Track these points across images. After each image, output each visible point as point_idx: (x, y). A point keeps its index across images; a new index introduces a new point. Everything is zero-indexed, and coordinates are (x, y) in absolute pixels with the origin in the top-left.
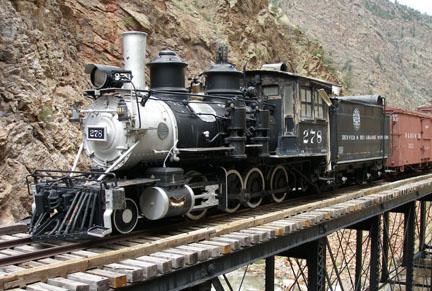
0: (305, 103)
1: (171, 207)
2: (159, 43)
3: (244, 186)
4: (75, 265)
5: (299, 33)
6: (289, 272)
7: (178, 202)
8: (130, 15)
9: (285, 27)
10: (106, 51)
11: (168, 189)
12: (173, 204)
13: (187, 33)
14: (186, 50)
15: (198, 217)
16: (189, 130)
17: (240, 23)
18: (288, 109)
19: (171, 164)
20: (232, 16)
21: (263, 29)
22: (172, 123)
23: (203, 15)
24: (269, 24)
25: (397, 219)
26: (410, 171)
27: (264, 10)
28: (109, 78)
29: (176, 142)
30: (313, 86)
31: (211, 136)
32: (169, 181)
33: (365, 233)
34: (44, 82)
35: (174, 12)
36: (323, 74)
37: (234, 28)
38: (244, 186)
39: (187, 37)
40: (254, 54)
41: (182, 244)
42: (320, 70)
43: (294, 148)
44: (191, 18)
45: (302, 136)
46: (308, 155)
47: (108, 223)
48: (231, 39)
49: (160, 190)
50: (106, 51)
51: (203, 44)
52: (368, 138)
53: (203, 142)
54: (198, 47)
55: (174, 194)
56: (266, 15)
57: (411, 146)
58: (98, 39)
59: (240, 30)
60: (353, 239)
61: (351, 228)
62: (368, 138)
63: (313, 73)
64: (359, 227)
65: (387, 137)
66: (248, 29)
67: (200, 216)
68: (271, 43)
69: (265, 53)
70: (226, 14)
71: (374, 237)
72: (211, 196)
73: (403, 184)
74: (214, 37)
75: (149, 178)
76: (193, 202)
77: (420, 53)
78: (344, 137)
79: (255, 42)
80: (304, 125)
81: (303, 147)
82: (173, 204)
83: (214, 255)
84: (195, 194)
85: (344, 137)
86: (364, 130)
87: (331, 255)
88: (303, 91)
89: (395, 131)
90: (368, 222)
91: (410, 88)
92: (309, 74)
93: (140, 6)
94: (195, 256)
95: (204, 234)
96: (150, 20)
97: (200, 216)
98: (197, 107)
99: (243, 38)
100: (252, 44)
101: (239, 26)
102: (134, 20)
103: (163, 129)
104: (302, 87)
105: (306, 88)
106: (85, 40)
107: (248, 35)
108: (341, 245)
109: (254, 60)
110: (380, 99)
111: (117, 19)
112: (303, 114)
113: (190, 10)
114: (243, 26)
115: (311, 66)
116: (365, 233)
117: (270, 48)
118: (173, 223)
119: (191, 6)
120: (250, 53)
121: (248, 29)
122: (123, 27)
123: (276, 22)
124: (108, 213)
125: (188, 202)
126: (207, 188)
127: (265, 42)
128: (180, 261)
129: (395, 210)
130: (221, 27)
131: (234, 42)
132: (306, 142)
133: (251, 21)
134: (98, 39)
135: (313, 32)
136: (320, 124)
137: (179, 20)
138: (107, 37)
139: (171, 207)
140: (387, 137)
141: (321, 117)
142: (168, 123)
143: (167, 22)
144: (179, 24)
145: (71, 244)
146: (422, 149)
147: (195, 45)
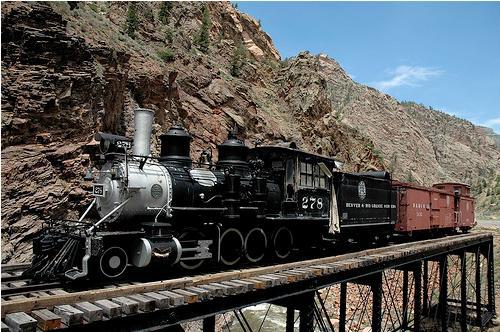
0: (306, 174)
1: (154, 257)
3: (244, 243)
4: (18, 305)
5: (355, 133)
6: (271, 316)
7: (165, 253)
8: (229, 116)
9: (345, 127)
10: (211, 141)
11: (152, 241)
12: (157, 254)
15: (192, 268)
16: (184, 191)
18: (289, 178)
19: (163, 218)
20: (305, 119)
21: (327, 128)
22: (166, 182)
23: (284, 117)
24: (332, 124)
25: (433, 266)
26: (420, 235)
28: (111, 145)
29: (170, 200)
30: (313, 160)
31: (206, 198)
32: (156, 233)
33: (410, 273)
35: (261, 114)
36: (372, 161)
38: (244, 243)
42: (370, 158)
43: (293, 212)
44: (275, 120)
45: (300, 203)
46: (307, 218)
47: (85, 267)
48: (303, 136)
49: (146, 242)
50: (211, 141)
52: (375, 206)
53: (199, 202)
55: (158, 246)
57: (420, 214)
58: (207, 133)
60: (402, 275)
61: (400, 268)
62: (375, 206)
64: (406, 269)
65: (394, 206)
66: (316, 128)
67: (196, 266)
69: (328, 145)
71: (417, 278)
72: (203, 250)
73: (409, 246)
75: (139, 230)
76: (179, 255)
77: (449, 146)
78: (348, 205)
80: (303, 193)
81: (302, 211)
82: (157, 254)
83: (177, 304)
84: (183, 247)
85: (348, 205)
86: (370, 197)
87: (321, 300)
88: (303, 165)
89: (403, 202)
90: (411, 264)
93: (238, 111)
94: (153, 304)
95: (179, 283)
96: (244, 120)
97: (196, 266)
98: (195, 173)
102: (233, 120)
103: (157, 190)
104: (301, 160)
105: (307, 162)
106: (197, 133)
108: (392, 279)
109: (320, 151)
110: (387, 174)
111: (220, 119)
112: (303, 183)
114: (313, 126)
115: (363, 155)
116: (410, 273)
118: (161, 269)
123: (337, 123)
124: (86, 258)
125: (174, 251)
126: (200, 242)
127: (329, 138)
128: (134, 308)
129: (433, 259)
130: (297, 126)
132: (305, 207)
134: (207, 133)
135: (369, 132)
136: (320, 193)
138: (213, 132)
139: (154, 257)
140: (394, 206)
141: (323, 187)
142: (162, 185)
143: (257, 122)
146: (431, 218)
147: (276, 139)
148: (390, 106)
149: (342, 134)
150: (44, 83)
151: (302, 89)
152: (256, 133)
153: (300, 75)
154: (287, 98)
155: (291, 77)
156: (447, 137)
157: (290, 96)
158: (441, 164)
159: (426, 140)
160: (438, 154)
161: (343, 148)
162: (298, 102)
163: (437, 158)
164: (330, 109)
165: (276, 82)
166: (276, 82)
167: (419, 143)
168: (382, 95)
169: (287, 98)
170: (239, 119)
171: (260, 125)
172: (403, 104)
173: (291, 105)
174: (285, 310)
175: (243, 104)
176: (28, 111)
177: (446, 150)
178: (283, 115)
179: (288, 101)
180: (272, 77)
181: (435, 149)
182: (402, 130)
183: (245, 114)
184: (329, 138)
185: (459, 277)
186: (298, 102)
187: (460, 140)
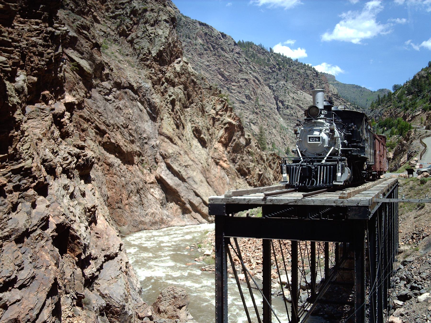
2: (97, 85)
13: (119, 77)
14: (118, 92)
17: (160, 70)
20: (155, 65)
21: (178, 75)
23: (128, 62)
24: (184, 71)
27: (179, 59)
34: (213, 112)
37: (155, 74)
39: (119, 81)
40: (174, 97)
41: (363, 191)
42: (226, 110)
48: (154, 84)
51: (131, 87)
54: (127, 90)
56: (181, 64)
59: (161, 75)
63: (220, 113)
66: (168, 75)
68: (186, 88)
69: (182, 96)
70: (149, 62)
74: (140, 81)
77: (292, 95)
79: (174, 86)
91: (285, 125)
92: (217, 114)
93: (82, 53)
96: (90, 65)
99: (163, 83)
100: (172, 88)
101: (159, 73)
102: (78, 65)
107: (167, 80)
113: (116, 57)
114: (164, 73)
117: (186, 92)
119: (117, 54)
120: (170, 96)
121: (168, 75)
122: (69, 70)
127: (181, 86)
130: (145, 72)
131: (156, 86)
133: (170, 68)
137: (112, 67)
144: (112, 70)
145: (228, 255)
147: (125, 88)
148: (225, 47)
149: (195, 83)
150: (45, 39)
151: (149, 28)
152: (102, 81)
153: (145, 10)
154: (129, 38)
155: (134, 12)
156: (289, 85)
157: (133, 35)
158: (284, 116)
159: (267, 88)
160: (280, 104)
161: (196, 99)
162: (145, 43)
163: (278, 108)
164: (182, 54)
165: (115, 17)
166: (115, 17)
167: (259, 91)
168: (216, 33)
169: (129, 38)
170: (85, 64)
171: (107, 71)
172: (240, 44)
173: (137, 46)
174: (259, 242)
175: (86, 45)
176: (38, 69)
177: (289, 99)
178: (129, 58)
179: (131, 42)
180: (107, 10)
181: (276, 98)
182: (240, 76)
183: (91, 59)
184: (181, 86)
185: (242, 287)
186: (145, 43)
187: (303, 88)
